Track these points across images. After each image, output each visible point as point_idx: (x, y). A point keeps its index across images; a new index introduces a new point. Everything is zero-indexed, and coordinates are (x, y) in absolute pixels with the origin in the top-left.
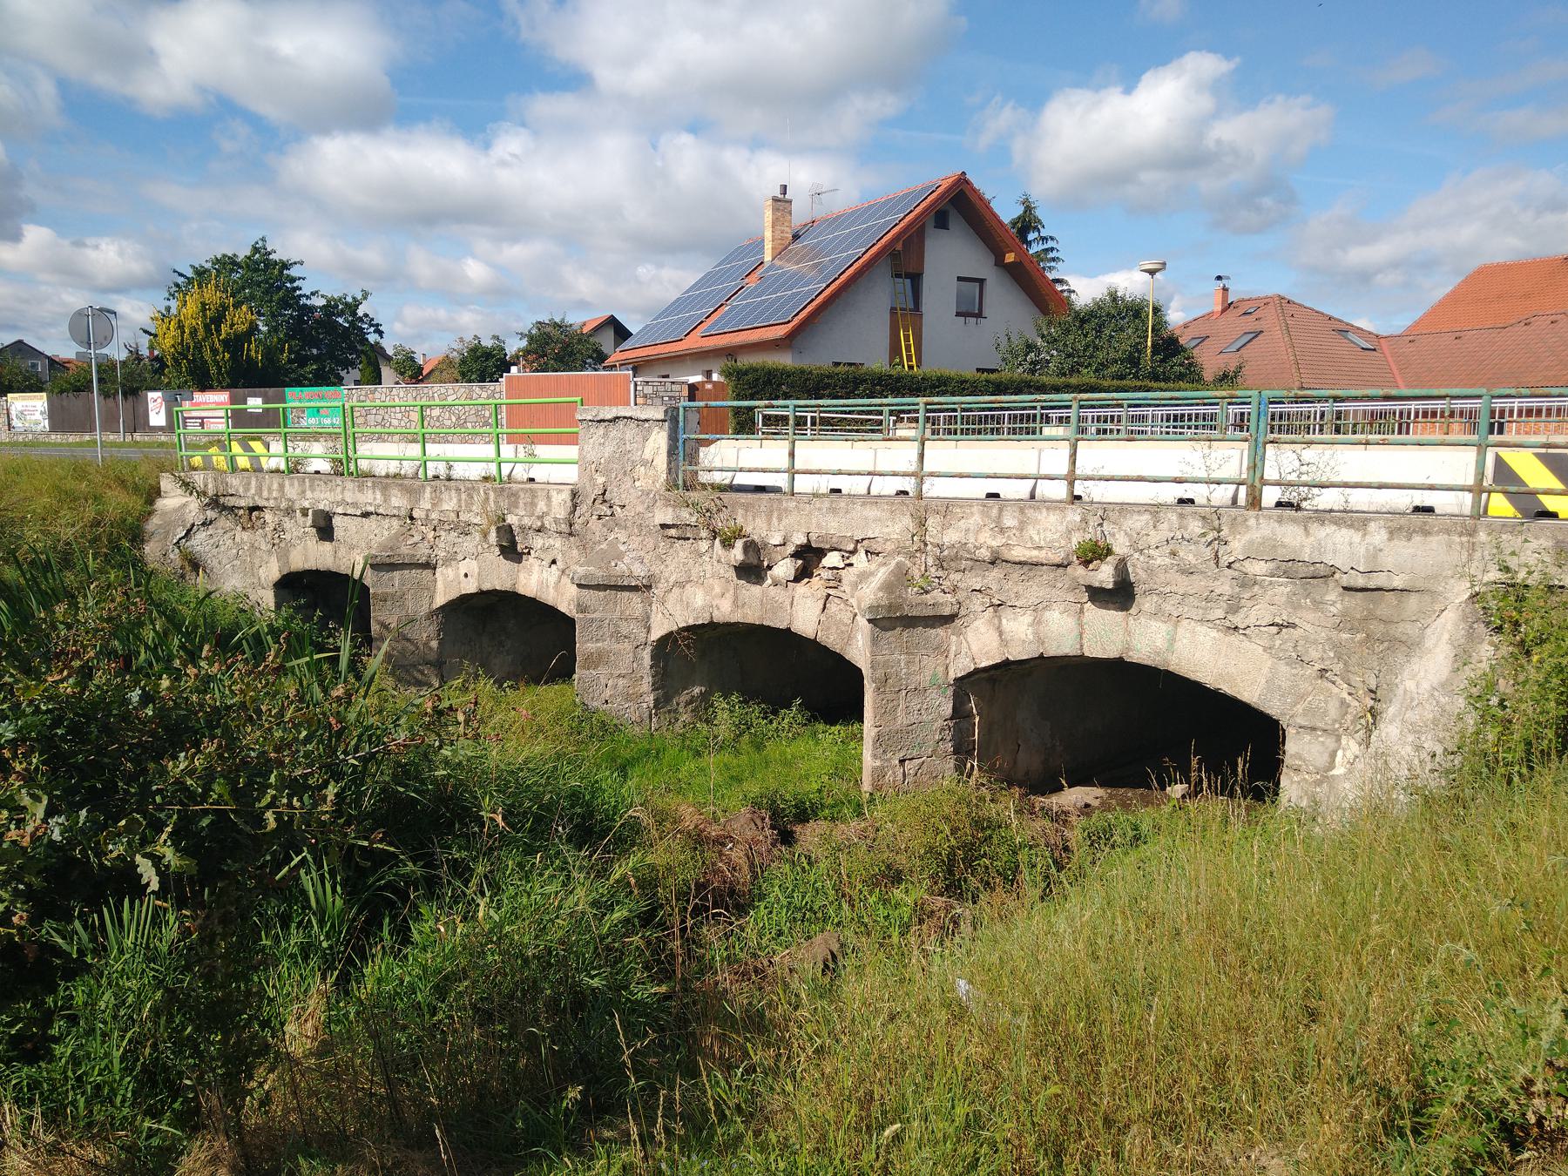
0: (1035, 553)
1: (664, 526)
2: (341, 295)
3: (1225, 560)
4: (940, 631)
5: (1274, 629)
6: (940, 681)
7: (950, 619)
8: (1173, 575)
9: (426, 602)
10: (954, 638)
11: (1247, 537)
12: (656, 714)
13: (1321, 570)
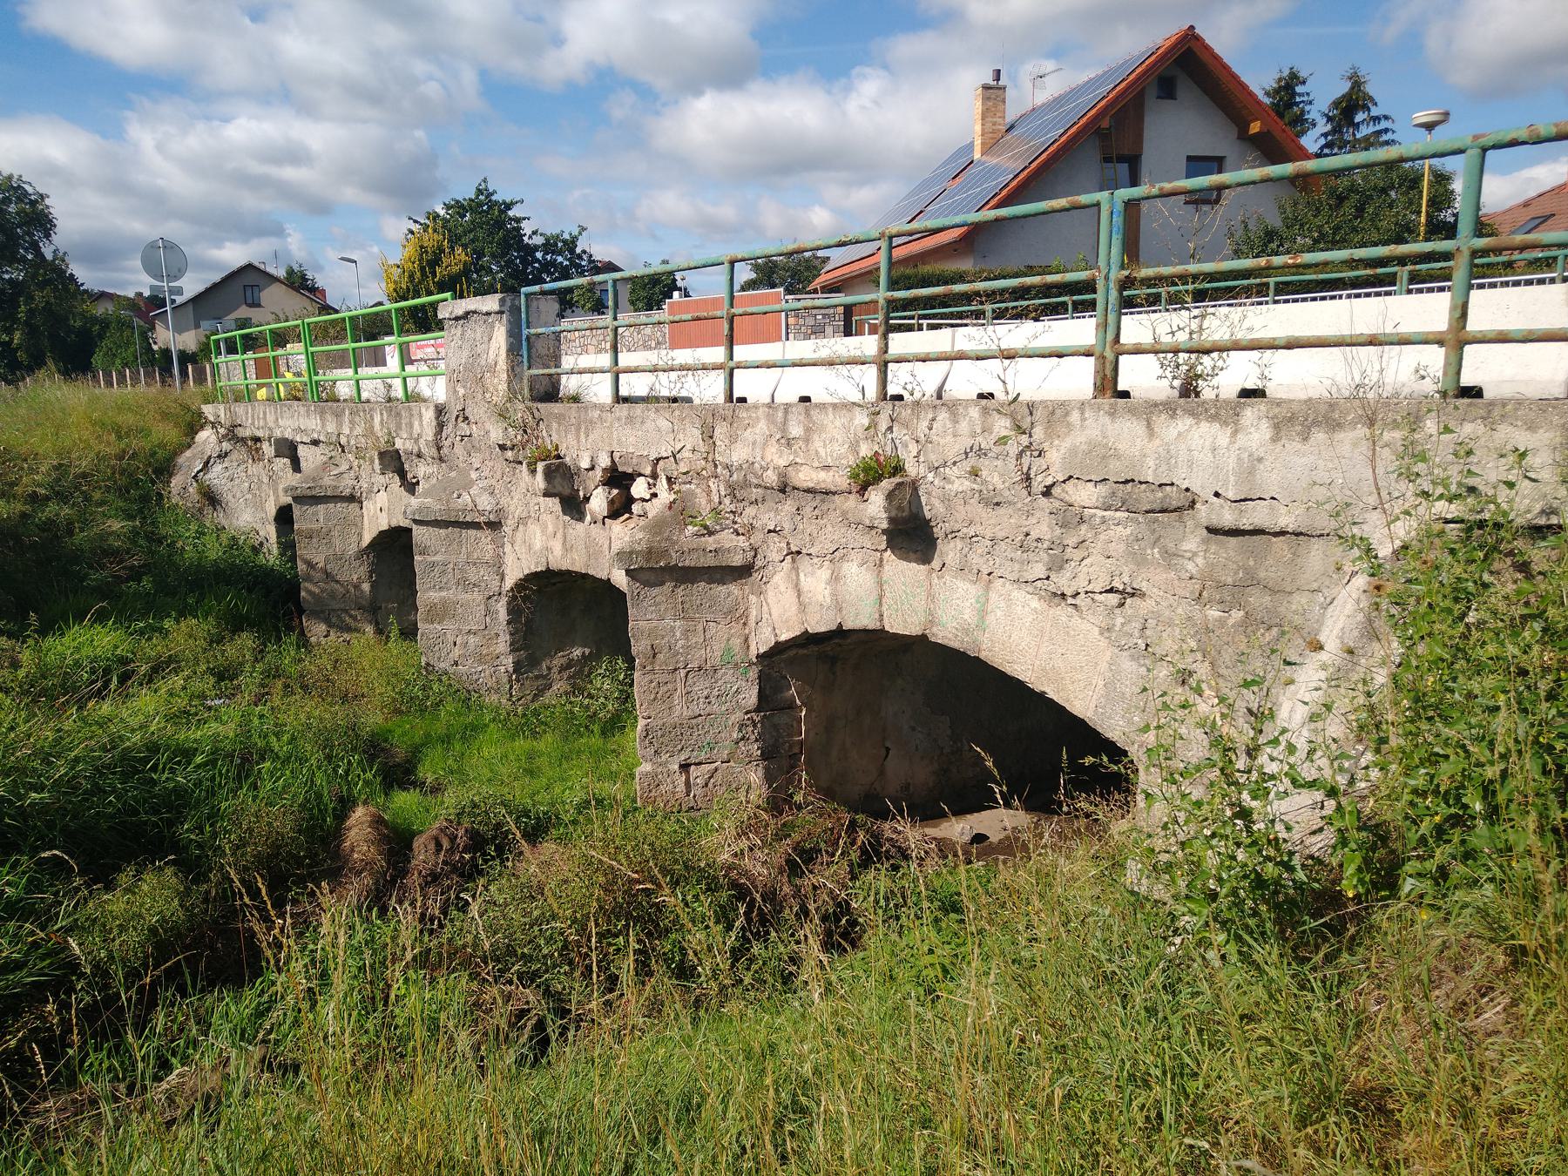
0: (822, 475)
1: (503, 447)
2: (558, 232)
3: (1039, 484)
4: (734, 588)
5: (1113, 599)
6: (738, 659)
7: (743, 572)
8: (976, 509)
9: (355, 538)
10: (753, 598)
11: (1067, 444)
12: (518, 680)
13: (1174, 498)
